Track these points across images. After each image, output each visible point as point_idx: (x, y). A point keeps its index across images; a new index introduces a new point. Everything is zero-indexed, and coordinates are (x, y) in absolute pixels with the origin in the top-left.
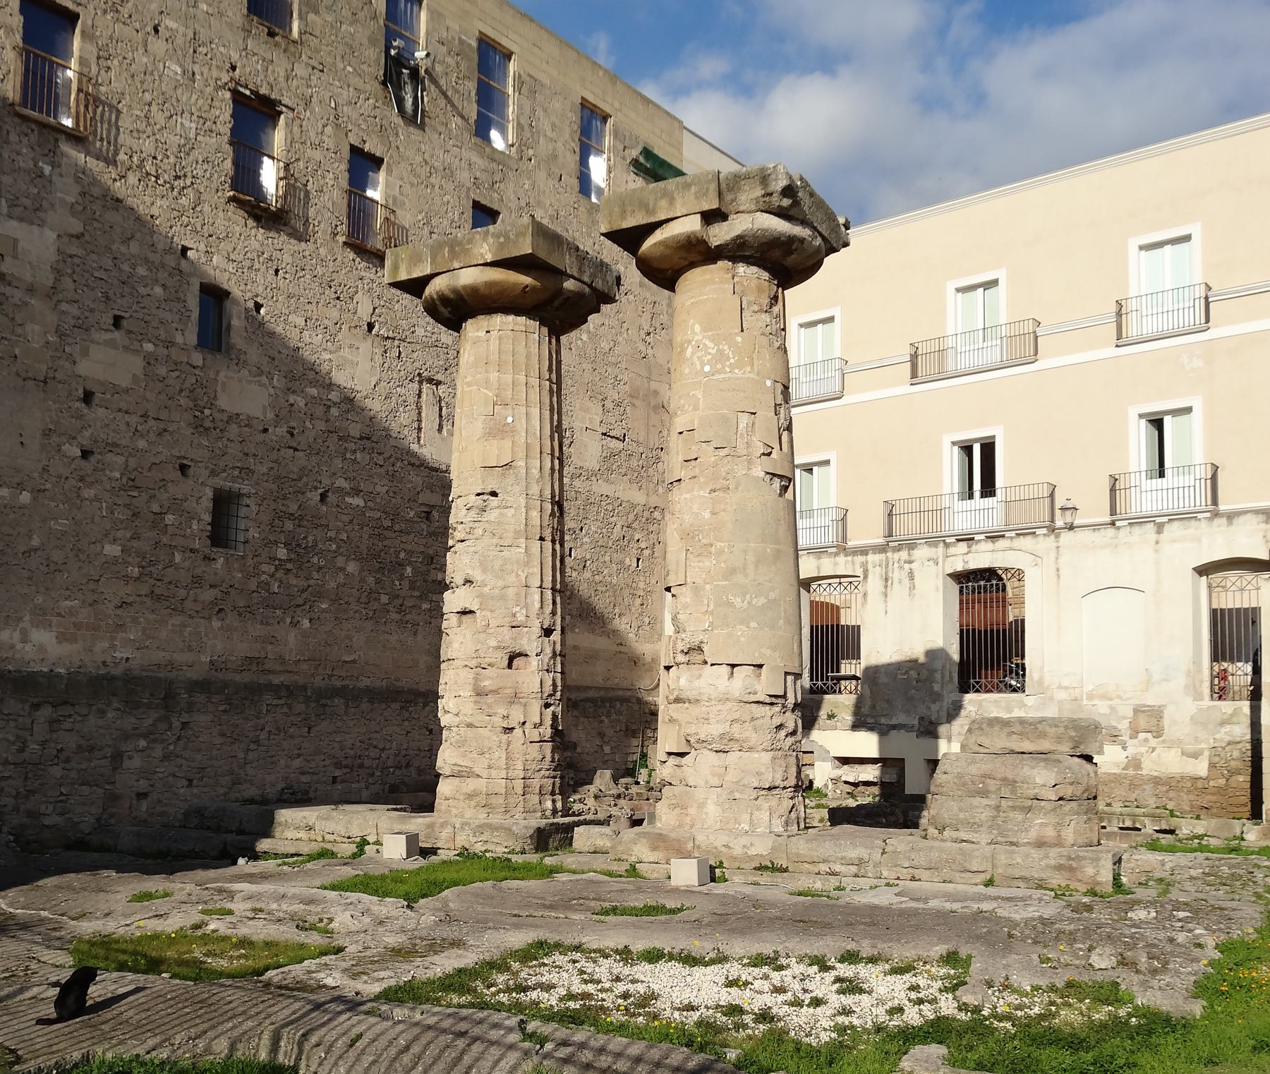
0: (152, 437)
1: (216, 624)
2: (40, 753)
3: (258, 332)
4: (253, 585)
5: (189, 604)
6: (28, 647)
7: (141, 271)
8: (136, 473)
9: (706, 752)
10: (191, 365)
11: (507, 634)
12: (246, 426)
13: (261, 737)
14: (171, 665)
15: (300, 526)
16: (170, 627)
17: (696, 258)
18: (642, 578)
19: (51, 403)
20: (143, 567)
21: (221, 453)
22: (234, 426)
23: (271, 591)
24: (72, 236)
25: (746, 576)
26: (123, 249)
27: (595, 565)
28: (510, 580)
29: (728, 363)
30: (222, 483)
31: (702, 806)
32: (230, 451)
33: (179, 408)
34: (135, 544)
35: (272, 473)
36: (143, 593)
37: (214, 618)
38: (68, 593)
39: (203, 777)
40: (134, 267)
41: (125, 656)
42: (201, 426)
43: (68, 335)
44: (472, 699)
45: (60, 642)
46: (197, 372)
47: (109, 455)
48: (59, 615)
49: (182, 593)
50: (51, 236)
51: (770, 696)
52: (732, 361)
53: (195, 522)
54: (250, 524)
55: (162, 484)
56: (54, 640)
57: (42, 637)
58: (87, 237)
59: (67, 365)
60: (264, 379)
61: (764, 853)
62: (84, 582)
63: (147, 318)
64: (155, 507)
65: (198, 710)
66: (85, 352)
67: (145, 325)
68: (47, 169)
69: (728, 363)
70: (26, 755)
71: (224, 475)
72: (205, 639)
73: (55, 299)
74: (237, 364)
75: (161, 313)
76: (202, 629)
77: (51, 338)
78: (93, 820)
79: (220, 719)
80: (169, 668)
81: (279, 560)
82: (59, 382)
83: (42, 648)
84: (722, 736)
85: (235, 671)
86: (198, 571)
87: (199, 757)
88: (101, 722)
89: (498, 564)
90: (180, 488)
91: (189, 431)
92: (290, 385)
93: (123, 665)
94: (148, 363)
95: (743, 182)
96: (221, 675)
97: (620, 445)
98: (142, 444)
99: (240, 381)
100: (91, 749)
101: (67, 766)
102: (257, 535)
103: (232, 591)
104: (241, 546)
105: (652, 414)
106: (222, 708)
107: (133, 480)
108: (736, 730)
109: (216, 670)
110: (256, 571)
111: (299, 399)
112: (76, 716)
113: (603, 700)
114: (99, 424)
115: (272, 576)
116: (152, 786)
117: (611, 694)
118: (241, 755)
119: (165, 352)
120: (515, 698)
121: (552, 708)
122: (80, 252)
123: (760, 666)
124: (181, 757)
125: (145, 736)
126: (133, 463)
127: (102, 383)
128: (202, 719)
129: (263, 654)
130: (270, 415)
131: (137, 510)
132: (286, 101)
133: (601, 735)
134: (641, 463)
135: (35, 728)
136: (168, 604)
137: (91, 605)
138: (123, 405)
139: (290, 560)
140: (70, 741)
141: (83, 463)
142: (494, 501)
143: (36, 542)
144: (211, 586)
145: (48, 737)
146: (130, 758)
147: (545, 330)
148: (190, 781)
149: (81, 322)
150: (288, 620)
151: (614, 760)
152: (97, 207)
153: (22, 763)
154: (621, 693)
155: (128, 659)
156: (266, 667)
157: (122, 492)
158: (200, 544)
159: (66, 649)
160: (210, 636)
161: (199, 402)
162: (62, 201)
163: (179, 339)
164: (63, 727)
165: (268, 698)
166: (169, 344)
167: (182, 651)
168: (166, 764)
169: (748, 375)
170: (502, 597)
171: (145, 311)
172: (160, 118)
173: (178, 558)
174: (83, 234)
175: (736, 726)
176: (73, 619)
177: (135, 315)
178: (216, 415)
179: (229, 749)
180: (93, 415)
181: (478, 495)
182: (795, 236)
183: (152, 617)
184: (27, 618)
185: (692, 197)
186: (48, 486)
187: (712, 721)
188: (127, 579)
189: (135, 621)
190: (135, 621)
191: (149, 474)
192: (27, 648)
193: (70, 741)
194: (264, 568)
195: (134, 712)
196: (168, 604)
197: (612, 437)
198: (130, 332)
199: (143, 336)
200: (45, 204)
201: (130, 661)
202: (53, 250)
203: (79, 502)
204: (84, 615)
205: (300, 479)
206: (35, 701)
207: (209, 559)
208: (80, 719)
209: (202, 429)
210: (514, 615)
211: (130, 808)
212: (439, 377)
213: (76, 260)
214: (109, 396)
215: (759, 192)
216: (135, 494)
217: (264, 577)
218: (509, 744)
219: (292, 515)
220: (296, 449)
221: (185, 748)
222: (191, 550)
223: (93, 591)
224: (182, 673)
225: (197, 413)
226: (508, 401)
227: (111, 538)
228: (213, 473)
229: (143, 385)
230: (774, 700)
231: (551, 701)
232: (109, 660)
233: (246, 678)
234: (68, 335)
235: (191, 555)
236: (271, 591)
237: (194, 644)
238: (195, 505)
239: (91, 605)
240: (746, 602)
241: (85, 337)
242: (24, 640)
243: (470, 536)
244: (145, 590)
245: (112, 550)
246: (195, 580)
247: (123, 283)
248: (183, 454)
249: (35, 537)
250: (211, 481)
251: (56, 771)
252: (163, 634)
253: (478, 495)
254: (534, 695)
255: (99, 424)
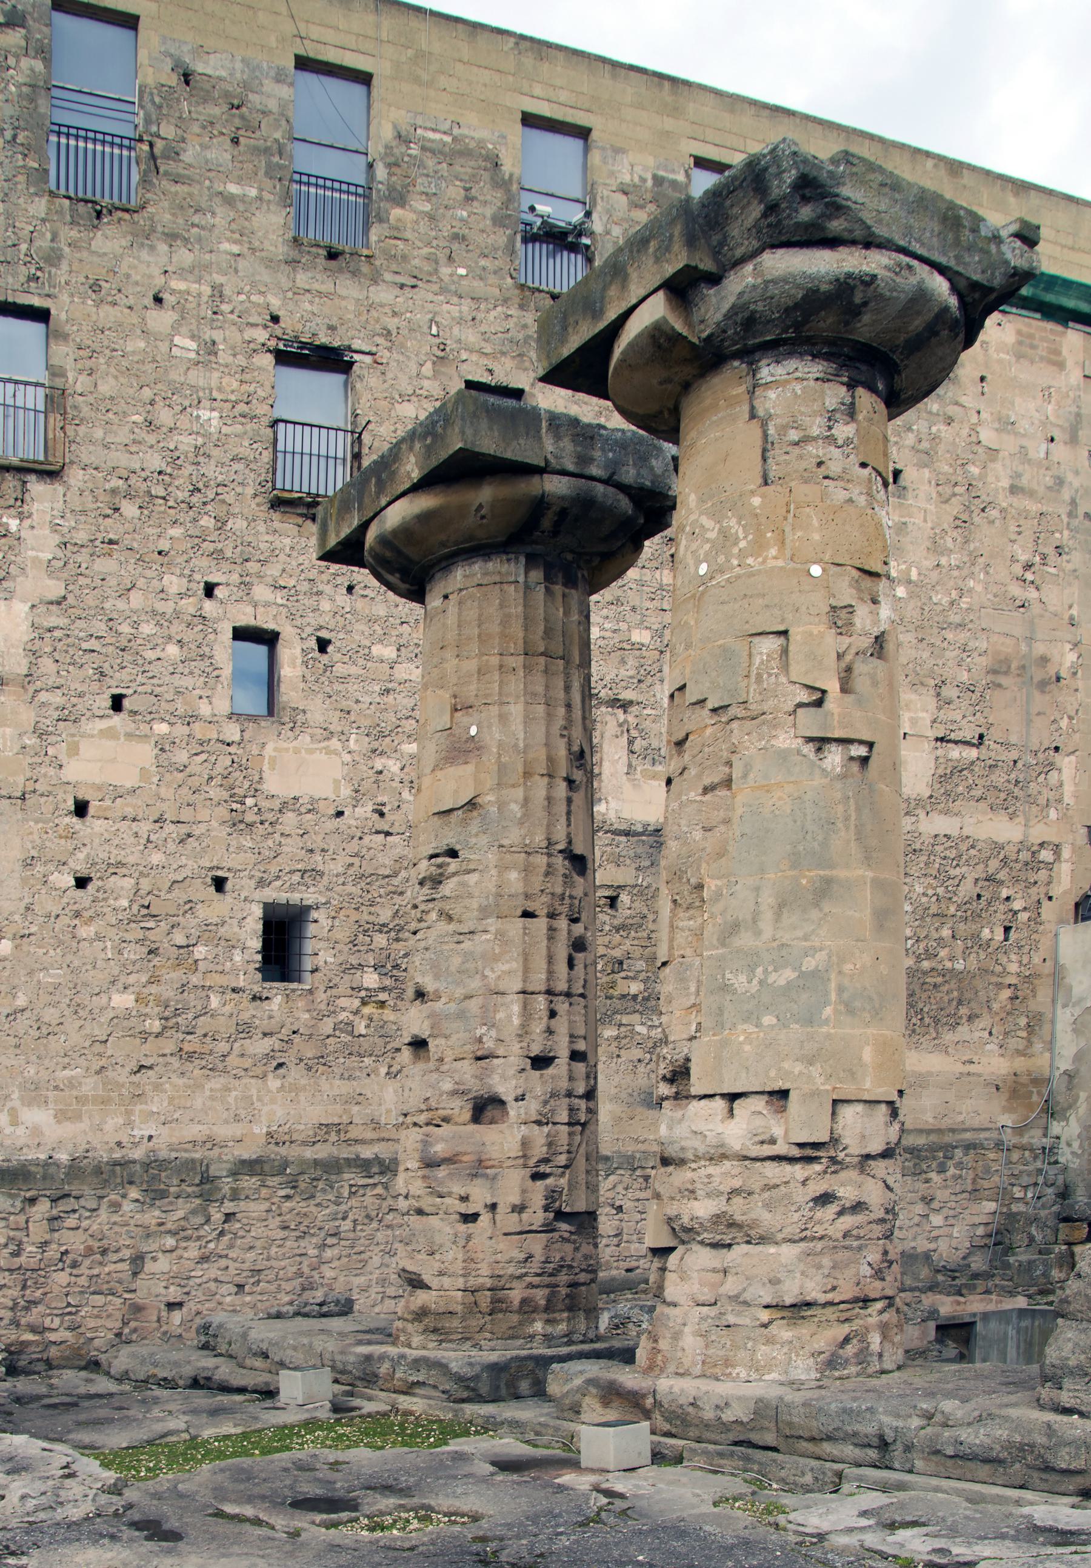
0: (171, 847)
1: (274, 1083)
2: (39, 1256)
3: (323, 679)
4: (327, 1027)
5: (233, 1060)
6: (20, 1131)
7: (147, 629)
8: (150, 897)
9: (696, 1247)
10: (223, 742)
11: (467, 1070)
12: (309, 811)
13: (342, 1229)
14: (211, 1142)
15: (397, 940)
16: (208, 1093)
17: (687, 371)
18: (1013, 957)
19: (32, 823)
20: (166, 1019)
21: (273, 854)
22: (290, 814)
23: (356, 1033)
24: (52, 603)
25: (758, 933)
26: (121, 605)
27: (922, 945)
28: (473, 986)
29: (735, 551)
30: (274, 895)
31: (677, 1336)
32: (285, 849)
33: (208, 803)
34: (153, 989)
35: (350, 872)
36: (167, 1051)
37: (270, 1076)
38: (67, 1060)
39: (259, 1281)
40: (136, 625)
41: (147, 1133)
42: (241, 822)
43: (51, 733)
44: (420, 1173)
45: (59, 1122)
46: (232, 749)
47: (113, 879)
48: (56, 1088)
49: (222, 1047)
50: (21, 608)
51: (801, 1145)
52: (742, 544)
53: (238, 951)
54: (322, 945)
55: (187, 907)
56: (52, 1120)
57: (39, 1117)
58: (71, 600)
59: (51, 772)
60: (335, 743)
61: (745, 1420)
62: (87, 1044)
63: (158, 690)
64: (179, 939)
65: (247, 1197)
66: (74, 751)
67: (155, 700)
68: (13, 524)
69: (735, 551)
70: (22, 1259)
71: (279, 883)
72: (257, 1104)
73: (31, 689)
74: (292, 729)
75: (178, 681)
76: (254, 1092)
77: (30, 741)
78: (111, 1336)
79: (279, 1207)
80: (209, 1145)
81: (367, 989)
82: (42, 795)
83: (36, 1131)
84: (717, 1218)
85: (304, 1143)
86: (245, 1016)
87: (250, 1256)
88: (116, 1218)
89: (456, 961)
90: (215, 907)
91: (224, 831)
92: (375, 745)
93: (145, 1146)
94: (162, 749)
95: (728, 203)
96: (283, 1151)
97: (973, 753)
98: (156, 858)
99: (297, 751)
100: (104, 1252)
101: (75, 1272)
102: (330, 960)
103: (296, 1038)
104: (307, 976)
105: (1037, 694)
106: (282, 1193)
107: (148, 907)
108: (737, 1208)
109: (277, 1144)
110: (332, 1008)
111: (391, 762)
112: (82, 1211)
113: (933, 1149)
114: (97, 841)
115: (356, 1012)
116: (187, 1293)
117: (948, 1138)
118: (312, 1252)
119: (186, 730)
120: (480, 1168)
121: (550, 1181)
122: (62, 622)
123: (784, 1094)
124: (226, 1256)
125: (173, 1233)
126: (145, 884)
127: (99, 788)
128: (256, 1208)
129: (345, 1119)
130: (346, 791)
131: (154, 946)
132: (357, 344)
133: (927, 1200)
134: (1013, 776)
135: (31, 1228)
136: (204, 1063)
137: (98, 1073)
138: (130, 811)
139: (383, 989)
140: (76, 1242)
141: (80, 893)
142: (453, 865)
143: (21, 1001)
144: (265, 1035)
145: (47, 1237)
146: (154, 1259)
147: (537, 575)
148: (240, 1287)
149: (66, 712)
150: (383, 1070)
151: (950, 1236)
152: (83, 557)
153: (19, 1268)
154: (968, 1135)
155: (150, 1137)
156: (352, 1135)
157: (133, 925)
158: (249, 978)
159: (68, 1130)
160: (266, 1099)
161: (236, 791)
162: (35, 560)
163: (205, 709)
164: (66, 1225)
165: (350, 1177)
166: (191, 719)
167: (226, 1122)
168: (205, 1266)
169: (771, 563)
170: (461, 1015)
171: (155, 681)
172: (165, 417)
173: (215, 1001)
174: (65, 598)
175: (737, 1200)
176: (75, 1093)
177: (140, 689)
178: (265, 804)
179: (296, 1244)
180: (89, 830)
181: (432, 857)
182: (849, 275)
183: (181, 1082)
184: (15, 1096)
185: (651, 261)
186: (34, 929)
187: (700, 1193)
188: (145, 1036)
189: (157, 1087)
190: (157, 1087)
191: (168, 896)
192: (18, 1133)
193: (76, 1242)
194: (343, 1002)
195: (157, 1203)
196: (204, 1063)
197: (956, 742)
198: (135, 713)
199: (153, 716)
200: (13, 569)
201: (154, 1140)
202: (25, 626)
203: (75, 945)
204: (90, 1086)
205: (395, 874)
206: (28, 1195)
207: (260, 999)
208: (88, 1214)
209: (242, 826)
210: (480, 1040)
211: (159, 1321)
212: (627, 695)
213: (58, 634)
214: (108, 803)
215: (756, 210)
216: (151, 924)
217: (343, 1016)
218: (469, 1238)
219: (383, 925)
220: (388, 834)
221: (231, 1246)
222: (234, 990)
223: (100, 1055)
224: (226, 1150)
225: (235, 806)
226: (472, 700)
227: (120, 986)
228: (262, 883)
229: (155, 780)
230: (809, 1152)
231: (544, 1169)
232: (125, 1140)
233: (322, 1152)
234: (51, 733)
235: (234, 995)
236: (356, 1033)
237: (242, 1113)
238: (236, 929)
239: (98, 1073)
240: (755, 982)
241: (73, 731)
242: (15, 1122)
243: (423, 925)
244: (169, 1047)
245: (123, 1001)
246: (240, 1028)
247: (123, 650)
248: (215, 863)
249: (20, 994)
250: (258, 895)
251: (62, 1278)
252: (198, 1103)
253: (432, 857)
254: (510, 1163)
255: (97, 841)
